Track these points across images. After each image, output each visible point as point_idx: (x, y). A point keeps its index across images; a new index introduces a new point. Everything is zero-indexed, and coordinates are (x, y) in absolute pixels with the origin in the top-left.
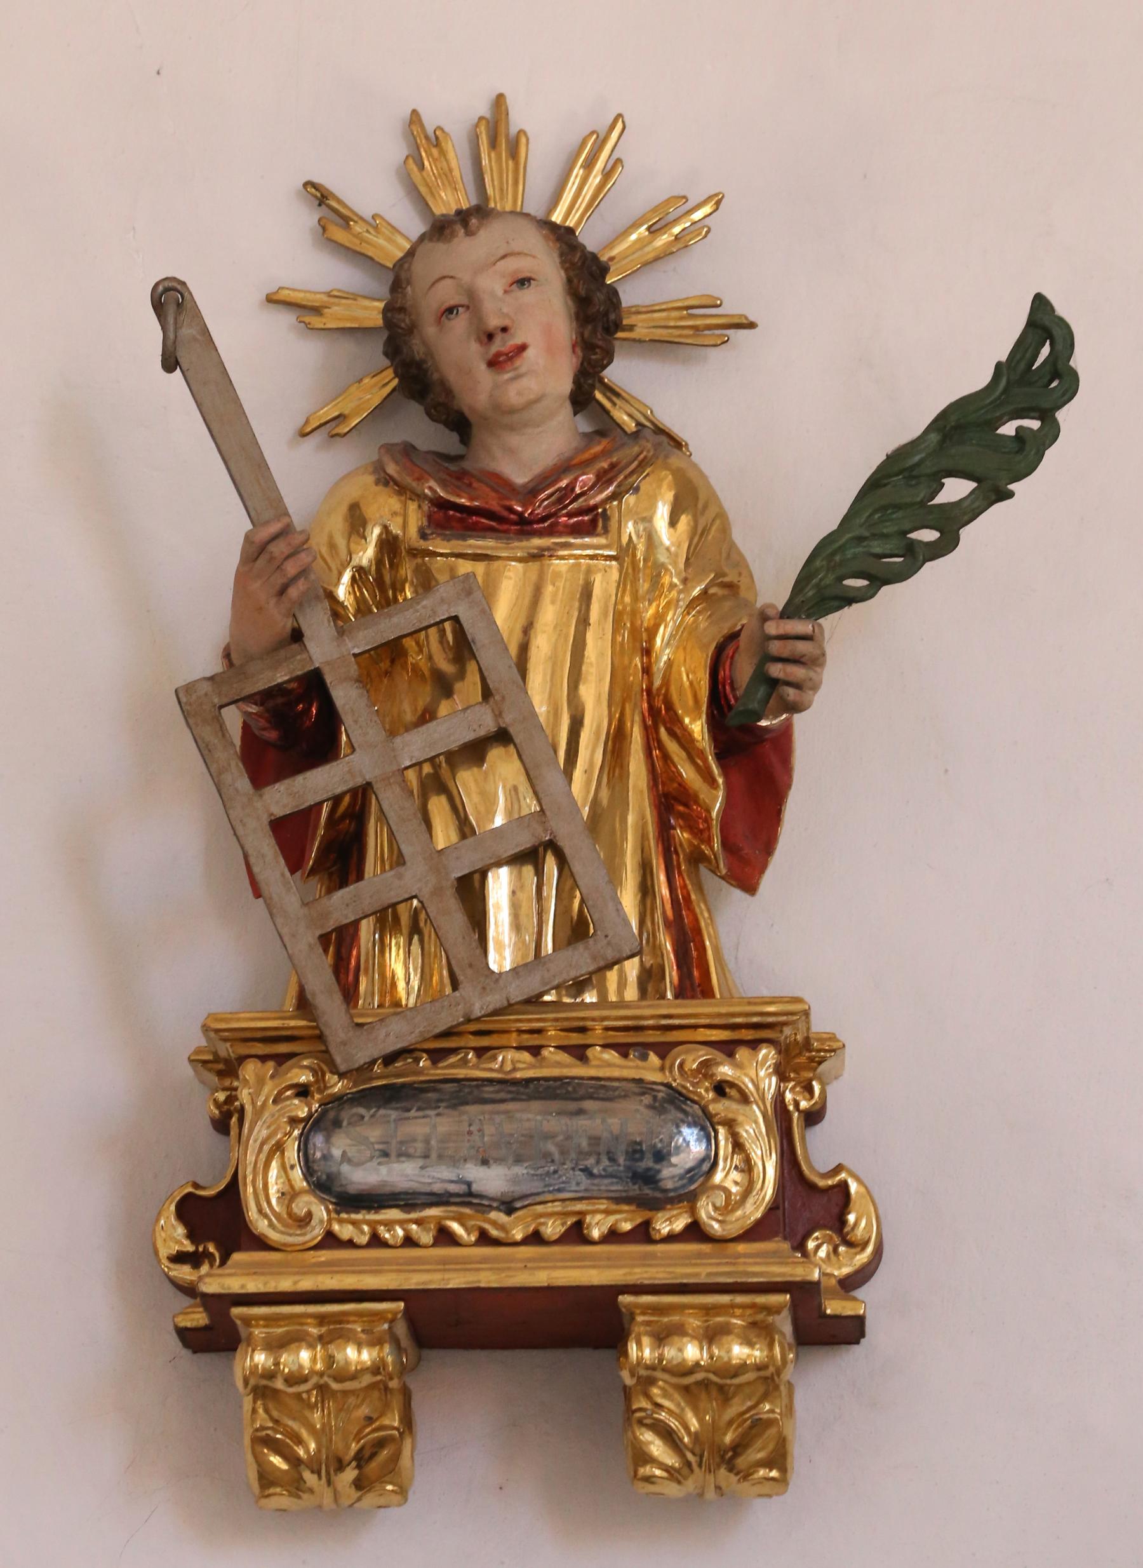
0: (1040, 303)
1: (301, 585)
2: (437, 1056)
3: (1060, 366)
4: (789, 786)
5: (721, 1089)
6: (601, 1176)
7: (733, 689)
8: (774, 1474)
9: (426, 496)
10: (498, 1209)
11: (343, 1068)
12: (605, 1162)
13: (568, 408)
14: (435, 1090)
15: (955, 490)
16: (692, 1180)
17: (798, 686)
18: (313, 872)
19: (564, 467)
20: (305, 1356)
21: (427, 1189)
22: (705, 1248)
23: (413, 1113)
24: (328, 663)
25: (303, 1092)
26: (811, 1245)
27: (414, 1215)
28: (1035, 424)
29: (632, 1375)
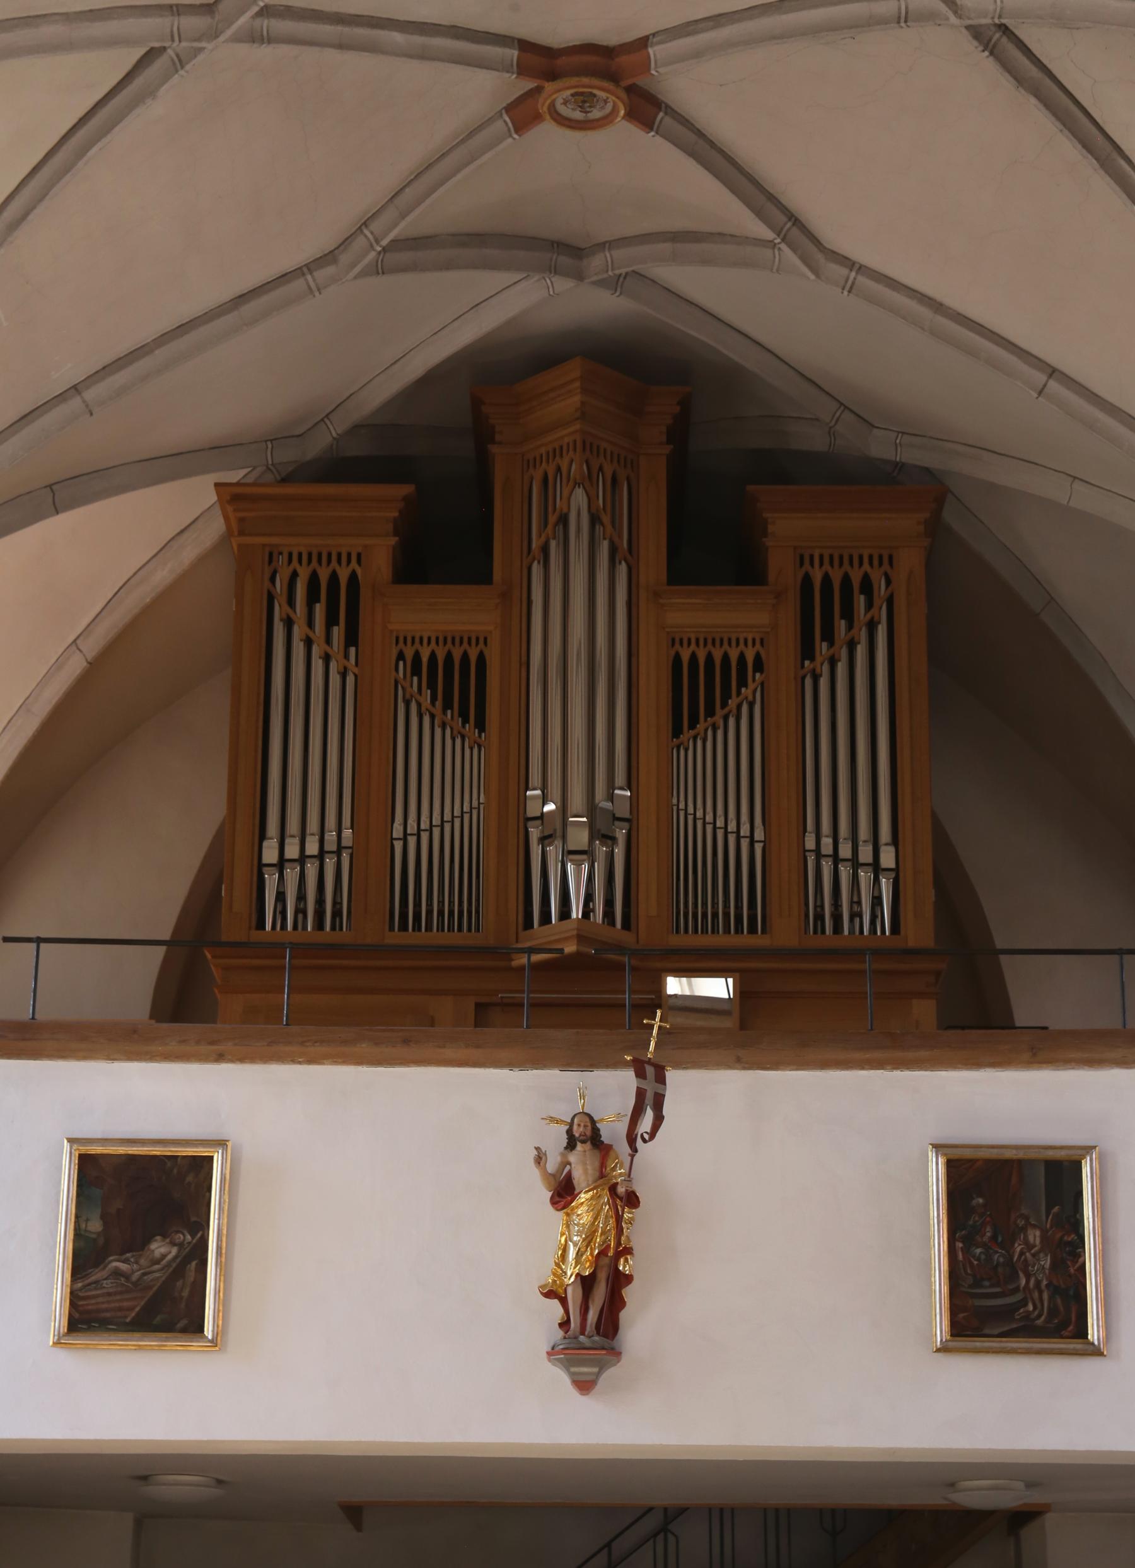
29: (978, 1221)
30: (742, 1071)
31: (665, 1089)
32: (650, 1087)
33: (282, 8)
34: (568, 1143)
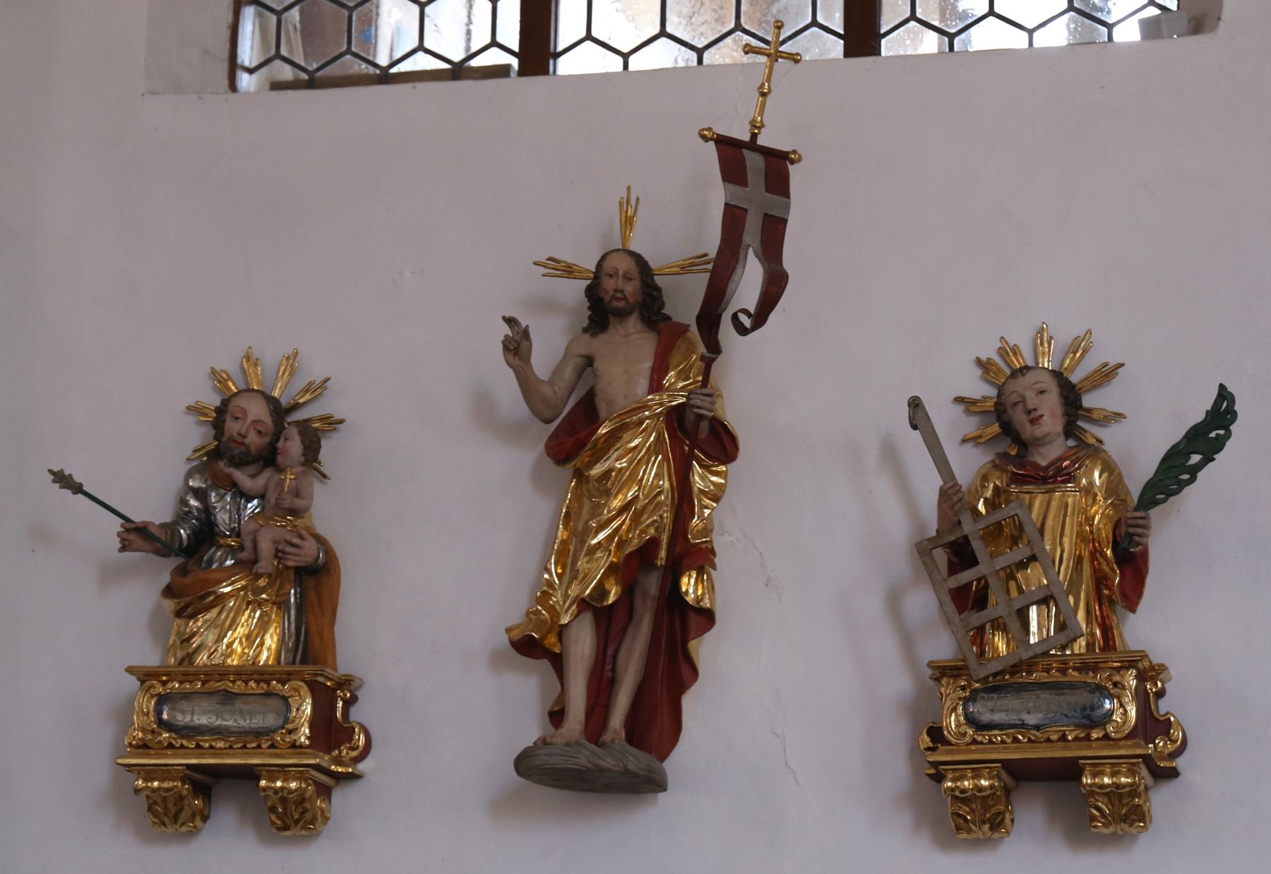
0: (1222, 387)
1: (959, 504)
2: (1012, 674)
3: (1230, 409)
4: (1147, 573)
5: (1115, 685)
6: (1071, 717)
7: (1120, 537)
8: (1142, 824)
9: (1009, 471)
10: (1034, 730)
11: (975, 679)
12: (1072, 712)
13: (1062, 437)
14: (1011, 687)
15: (1195, 458)
16: (1105, 718)
17: (1140, 536)
18: (972, 609)
19: (1061, 459)
20: (966, 783)
21: (1007, 723)
22: (1111, 743)
23: (1003, 695)
24: (970, 533)
25: (963, 688)
26: (1157, 741)
27: (1003, 732)
28: (1222, 432)
29: (1084, 789)
30: (1155, 41)
31: (787, 208)
32: (755, 195)
33: (584, 769)
34: (590, 318)
